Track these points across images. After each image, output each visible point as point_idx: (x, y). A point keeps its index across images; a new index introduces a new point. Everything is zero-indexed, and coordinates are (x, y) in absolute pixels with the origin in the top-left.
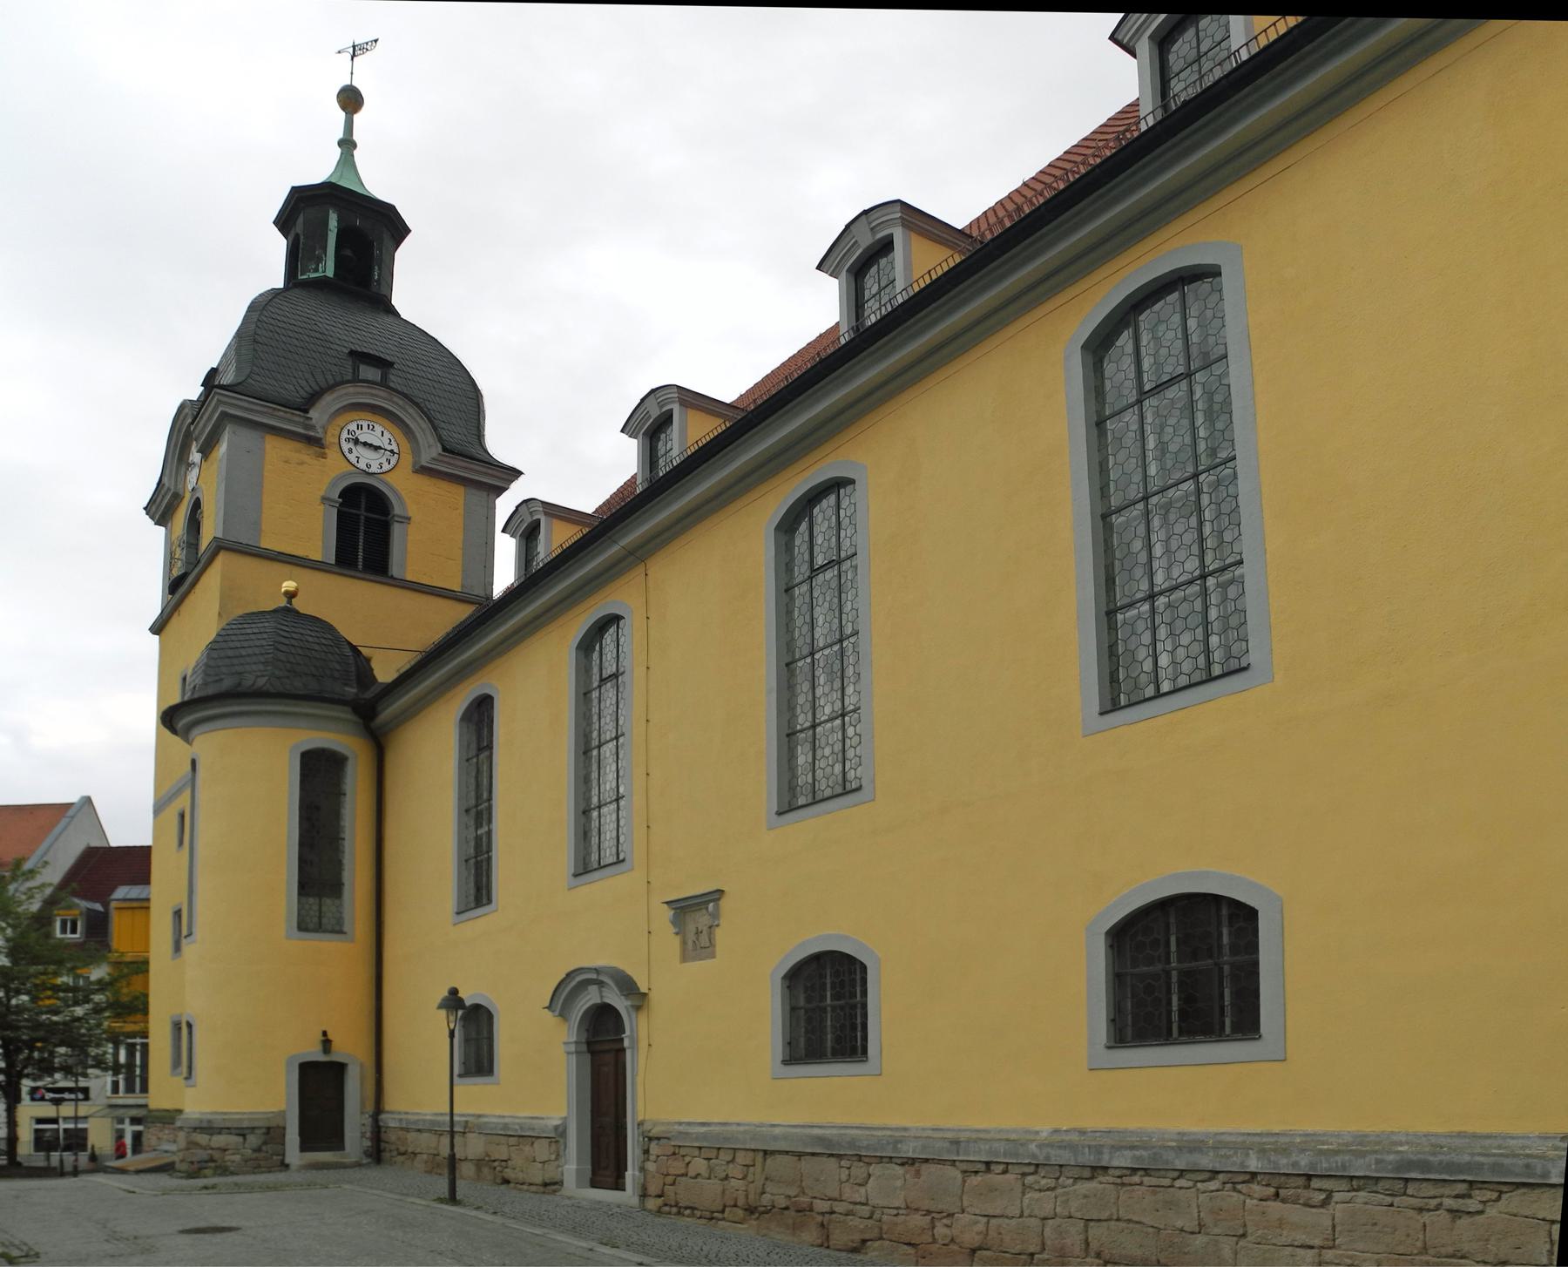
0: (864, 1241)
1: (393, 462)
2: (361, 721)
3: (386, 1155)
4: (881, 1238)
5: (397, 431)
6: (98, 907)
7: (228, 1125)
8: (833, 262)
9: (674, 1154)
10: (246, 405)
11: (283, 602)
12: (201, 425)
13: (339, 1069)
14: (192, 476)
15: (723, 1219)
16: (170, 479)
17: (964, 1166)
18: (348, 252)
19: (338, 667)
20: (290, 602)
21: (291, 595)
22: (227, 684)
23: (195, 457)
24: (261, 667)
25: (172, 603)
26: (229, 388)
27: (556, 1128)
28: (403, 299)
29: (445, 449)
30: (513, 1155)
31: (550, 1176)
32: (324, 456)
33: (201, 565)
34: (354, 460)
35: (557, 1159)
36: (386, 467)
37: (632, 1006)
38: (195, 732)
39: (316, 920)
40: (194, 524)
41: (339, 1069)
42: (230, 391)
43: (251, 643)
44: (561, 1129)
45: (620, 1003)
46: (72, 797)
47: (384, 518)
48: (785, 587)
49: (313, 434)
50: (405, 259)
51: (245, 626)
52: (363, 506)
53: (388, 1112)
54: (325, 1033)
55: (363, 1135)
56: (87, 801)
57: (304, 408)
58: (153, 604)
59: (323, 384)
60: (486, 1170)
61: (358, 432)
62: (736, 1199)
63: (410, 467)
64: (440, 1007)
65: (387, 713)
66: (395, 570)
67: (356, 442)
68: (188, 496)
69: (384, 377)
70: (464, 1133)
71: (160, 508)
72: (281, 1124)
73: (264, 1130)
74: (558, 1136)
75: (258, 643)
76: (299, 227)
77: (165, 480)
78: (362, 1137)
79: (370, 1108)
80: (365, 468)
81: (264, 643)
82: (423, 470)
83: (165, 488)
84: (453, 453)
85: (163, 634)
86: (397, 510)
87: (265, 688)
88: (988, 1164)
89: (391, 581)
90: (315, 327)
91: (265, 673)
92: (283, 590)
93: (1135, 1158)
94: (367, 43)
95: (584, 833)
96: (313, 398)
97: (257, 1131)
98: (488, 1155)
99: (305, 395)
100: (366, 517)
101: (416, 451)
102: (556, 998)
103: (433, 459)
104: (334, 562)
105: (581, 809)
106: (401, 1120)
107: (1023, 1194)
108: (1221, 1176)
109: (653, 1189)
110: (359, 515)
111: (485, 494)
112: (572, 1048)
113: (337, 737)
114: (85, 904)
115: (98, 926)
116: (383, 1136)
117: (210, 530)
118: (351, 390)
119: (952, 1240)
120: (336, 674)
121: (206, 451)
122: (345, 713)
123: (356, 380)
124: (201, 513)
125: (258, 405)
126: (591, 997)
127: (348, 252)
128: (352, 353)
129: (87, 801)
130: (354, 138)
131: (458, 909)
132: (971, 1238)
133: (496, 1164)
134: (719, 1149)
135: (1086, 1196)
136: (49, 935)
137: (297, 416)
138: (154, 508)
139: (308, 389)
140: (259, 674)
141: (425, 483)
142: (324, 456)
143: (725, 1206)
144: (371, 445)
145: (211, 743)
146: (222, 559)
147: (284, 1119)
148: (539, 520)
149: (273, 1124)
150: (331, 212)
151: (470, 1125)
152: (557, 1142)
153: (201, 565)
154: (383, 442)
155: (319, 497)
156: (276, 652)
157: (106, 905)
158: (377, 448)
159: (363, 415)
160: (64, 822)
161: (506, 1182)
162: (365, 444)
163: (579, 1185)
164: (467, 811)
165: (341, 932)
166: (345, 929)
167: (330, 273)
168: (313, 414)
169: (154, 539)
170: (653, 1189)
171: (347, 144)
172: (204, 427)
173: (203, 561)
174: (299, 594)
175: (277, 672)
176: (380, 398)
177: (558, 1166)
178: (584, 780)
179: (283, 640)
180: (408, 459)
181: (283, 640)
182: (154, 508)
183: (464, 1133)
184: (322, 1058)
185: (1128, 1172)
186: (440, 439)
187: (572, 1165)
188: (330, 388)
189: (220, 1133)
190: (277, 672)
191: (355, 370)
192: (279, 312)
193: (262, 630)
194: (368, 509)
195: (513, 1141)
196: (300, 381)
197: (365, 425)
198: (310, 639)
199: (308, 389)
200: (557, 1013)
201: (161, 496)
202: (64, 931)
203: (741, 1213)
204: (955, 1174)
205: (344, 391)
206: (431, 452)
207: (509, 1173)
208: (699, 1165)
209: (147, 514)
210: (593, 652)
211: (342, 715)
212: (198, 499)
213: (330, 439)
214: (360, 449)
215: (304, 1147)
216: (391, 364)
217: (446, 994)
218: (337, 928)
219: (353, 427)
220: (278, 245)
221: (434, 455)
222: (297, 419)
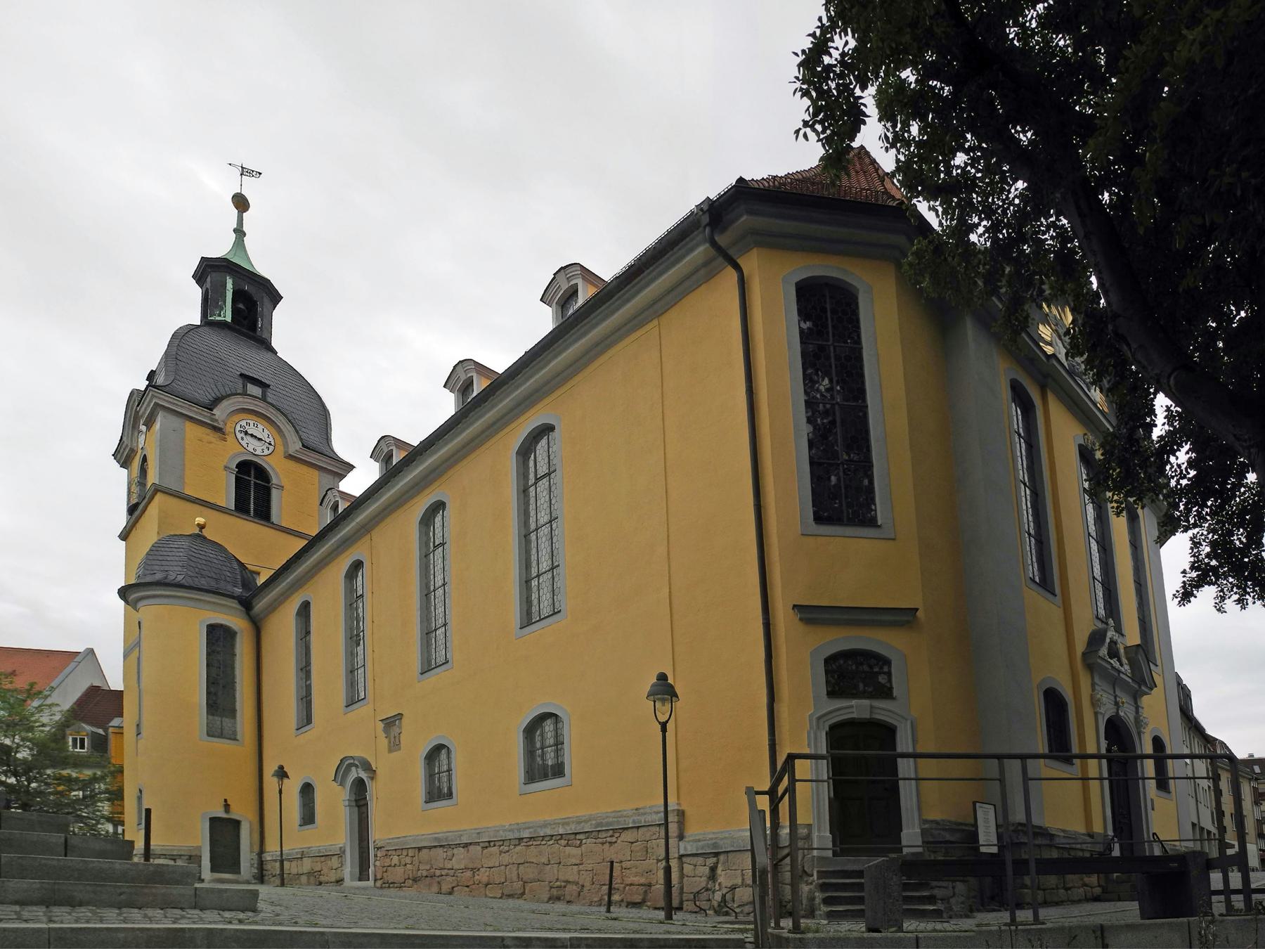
0: (453, 888)
1: (271, 450)
2: (244, 609)
3: (266, 878)
4: (458, 885)
5: (273, 430)
6: (101, 731)
7: (164, 852)
8: (452, 382)
9: (386, 855)
10: (170, 400)
11: (197, 531)
12: (143, 408)
13: (236, 824)
14: (142, 439)
15: (405, 887)
16: (127, 438)
17: (482, 845)
18: (241, 306)
19: (229, 575)
20: (201, 531)
21: (202, 527)
22: (158, 576)
23: (143, 428)
24: (180, 569)
25: (132, 521)
26: (160, 388)
27: (341, 848)
28: (279, 340)
29: (303, 446)
30: (324, 868)
31: (338, 877)
32: (225, 440)
33: (146, 500)
34: (245, 446)
35: (341, 867)
36: (266, 452)
37: (370, 777)
38: (140, 604)
39: (219, 731)
40: (143, 471)
41: (236, 824)
42: (158, 389)
43: (174, 554)
44: (343, 849)
45: (363, 775)
46: (80, 648)
47: (266, 484)
48: (424, 554)
49: (217, 425)
50: (280, 316)
51: (170, 542)
52: (253, 475)
53: (268, 852)
54: (226, 800)
55: (252, 865)
56: (91, 652)
57: (210, 407)
58: (121, 520)
59: (224, 394)
60: (312, 878)
61: (247, 427)
62: (409, 875)
63: (283, 454)
64: (273, 776)
65: (260, 605)
66: (274, 518)
67: (246, 433)
68: (140, 451)
69: (264, 394)
70: (302, 858)
71: (124, 455)
72: (199, 854)
73: (187, 857)
74: (341, 854)
75: (178, 554)
76: (208, 285)
77: (124, 439)
78: (251, 867)
79: (257, 849)
80: (252, 451)
81: (181, 554)
82: (290, 457)
83: (125, 444)
84: (309, 448)
85: (128, 540)
86: (274, 481)
87: (181, 582)
88: (489, 842)
89: (271, 525)
90: (216, 355)
91: (182, 573)
92: (196, 523)
93: (530, 833)
94: (253, 171)
95: (352, 684)
96: (216, 401)
97: (182, 857)
98: (313, 870)
99: (212, 399)
100: (255, 482)
101: (286, 444)
102: (337, 775)
103: (296, 451)
104: (234, 509)
105: (350, 670)
106: (272, 855)
107: (500, 854)
108: (554, 838)
109: (379, 877)
110: (250, 481)
111: (332, 477)
112: (347, 803)
113: (234, 620)
114: (89, 728)
115: (100, 744)
116: (265, 867)
117: (152, 478)
118: (241, 400)
119: (480, 882)
120: (228, 579)
121: (149, 423)
122: (234, 604)
123: (244, 394)
124: (147, 465)
125: (180, 402)
126: (353, 774)
127: (241, 306)
128: (242, 375)
129: (91, 652)
130: (244, 229)
131: (298, 725)
132: (485, 880)
133: (316, 874)
134: (402, 849)
135: (517, 853)
136: (65, 749)
137: (206, 412)
138: (119, 456)
139: (213, 395)
140: (179, 573)
141: (291, 465)
142: (225, 440)
143: (405, 880)
144: (256, 437)
145: (150, 611)
146: (159, 497)
147: (201, 851)
148: (338, 501)
149: (193, 854)
150: (228, 278)
151: (305, 853)
152: (341, 856)
153: (146, 500)
154: (264, 436)
155: (222, 466)
156: (189, 561)
157: (106, 730)
158: (260, 439)
159: (250, 416)
160: (73, 665)
161: (320, 884)
162: (252, 435)
163: (352, 880)
164: (301, 669)
165: (235, 739)
166: (238, 737)
167: (229, 319)
168: (215, 411)
169: (121, 476)
170: (379, 877)
171: (240, 232)
172: (146, 410)
173: (147, 497)
174: (207, 526)
175: (189, 573)
176: (261, 407)
177: (342, 870)
178: (351, 655)
179: (193, 554)
180: (280, 449)
181: (193, 554)
182: (119, 456)
183: (302, 858)
184: (225, 816)
185: (528, 840)
186: (301, 439)
187: (349, 869)
188: (228, 396)
189: (159, 858)
190: (189, 573)
191: (245, 387)
192: (192, 341)
193: (181, 547)
194: (256, 478)
195: (323, 859)
196: (208, 389)
197: (252, 423)
198: (211, 556)
199: (213, 395)
200: (339, 784)
201: (122, 449)
202: (75, 746)
203: (411, 881)
204: (479, 848)
205: (236, 400)
206: (295, 446)
207: (322, 879)
208: (395, 860)
209: (115, 459)
210: (1101, 647)
211: (234, 605)
212: (145, 455)
213: (228, 429)
214: (249, 438)
215: (213, 869)
216: (268, 386)
217: (277, 768)
218: (232, 737)
219: (243, 423)
220: (197, 292)
221: (298, 448)
222: (205, 413)
